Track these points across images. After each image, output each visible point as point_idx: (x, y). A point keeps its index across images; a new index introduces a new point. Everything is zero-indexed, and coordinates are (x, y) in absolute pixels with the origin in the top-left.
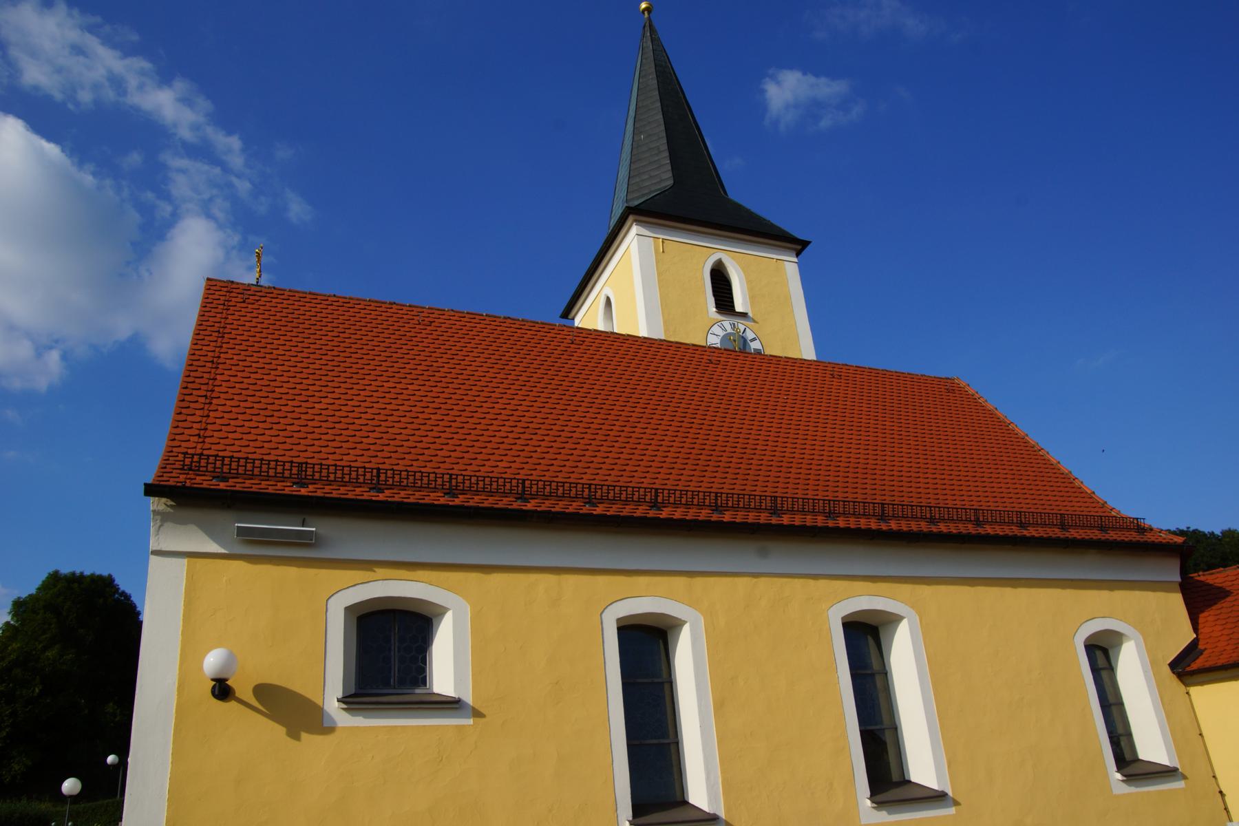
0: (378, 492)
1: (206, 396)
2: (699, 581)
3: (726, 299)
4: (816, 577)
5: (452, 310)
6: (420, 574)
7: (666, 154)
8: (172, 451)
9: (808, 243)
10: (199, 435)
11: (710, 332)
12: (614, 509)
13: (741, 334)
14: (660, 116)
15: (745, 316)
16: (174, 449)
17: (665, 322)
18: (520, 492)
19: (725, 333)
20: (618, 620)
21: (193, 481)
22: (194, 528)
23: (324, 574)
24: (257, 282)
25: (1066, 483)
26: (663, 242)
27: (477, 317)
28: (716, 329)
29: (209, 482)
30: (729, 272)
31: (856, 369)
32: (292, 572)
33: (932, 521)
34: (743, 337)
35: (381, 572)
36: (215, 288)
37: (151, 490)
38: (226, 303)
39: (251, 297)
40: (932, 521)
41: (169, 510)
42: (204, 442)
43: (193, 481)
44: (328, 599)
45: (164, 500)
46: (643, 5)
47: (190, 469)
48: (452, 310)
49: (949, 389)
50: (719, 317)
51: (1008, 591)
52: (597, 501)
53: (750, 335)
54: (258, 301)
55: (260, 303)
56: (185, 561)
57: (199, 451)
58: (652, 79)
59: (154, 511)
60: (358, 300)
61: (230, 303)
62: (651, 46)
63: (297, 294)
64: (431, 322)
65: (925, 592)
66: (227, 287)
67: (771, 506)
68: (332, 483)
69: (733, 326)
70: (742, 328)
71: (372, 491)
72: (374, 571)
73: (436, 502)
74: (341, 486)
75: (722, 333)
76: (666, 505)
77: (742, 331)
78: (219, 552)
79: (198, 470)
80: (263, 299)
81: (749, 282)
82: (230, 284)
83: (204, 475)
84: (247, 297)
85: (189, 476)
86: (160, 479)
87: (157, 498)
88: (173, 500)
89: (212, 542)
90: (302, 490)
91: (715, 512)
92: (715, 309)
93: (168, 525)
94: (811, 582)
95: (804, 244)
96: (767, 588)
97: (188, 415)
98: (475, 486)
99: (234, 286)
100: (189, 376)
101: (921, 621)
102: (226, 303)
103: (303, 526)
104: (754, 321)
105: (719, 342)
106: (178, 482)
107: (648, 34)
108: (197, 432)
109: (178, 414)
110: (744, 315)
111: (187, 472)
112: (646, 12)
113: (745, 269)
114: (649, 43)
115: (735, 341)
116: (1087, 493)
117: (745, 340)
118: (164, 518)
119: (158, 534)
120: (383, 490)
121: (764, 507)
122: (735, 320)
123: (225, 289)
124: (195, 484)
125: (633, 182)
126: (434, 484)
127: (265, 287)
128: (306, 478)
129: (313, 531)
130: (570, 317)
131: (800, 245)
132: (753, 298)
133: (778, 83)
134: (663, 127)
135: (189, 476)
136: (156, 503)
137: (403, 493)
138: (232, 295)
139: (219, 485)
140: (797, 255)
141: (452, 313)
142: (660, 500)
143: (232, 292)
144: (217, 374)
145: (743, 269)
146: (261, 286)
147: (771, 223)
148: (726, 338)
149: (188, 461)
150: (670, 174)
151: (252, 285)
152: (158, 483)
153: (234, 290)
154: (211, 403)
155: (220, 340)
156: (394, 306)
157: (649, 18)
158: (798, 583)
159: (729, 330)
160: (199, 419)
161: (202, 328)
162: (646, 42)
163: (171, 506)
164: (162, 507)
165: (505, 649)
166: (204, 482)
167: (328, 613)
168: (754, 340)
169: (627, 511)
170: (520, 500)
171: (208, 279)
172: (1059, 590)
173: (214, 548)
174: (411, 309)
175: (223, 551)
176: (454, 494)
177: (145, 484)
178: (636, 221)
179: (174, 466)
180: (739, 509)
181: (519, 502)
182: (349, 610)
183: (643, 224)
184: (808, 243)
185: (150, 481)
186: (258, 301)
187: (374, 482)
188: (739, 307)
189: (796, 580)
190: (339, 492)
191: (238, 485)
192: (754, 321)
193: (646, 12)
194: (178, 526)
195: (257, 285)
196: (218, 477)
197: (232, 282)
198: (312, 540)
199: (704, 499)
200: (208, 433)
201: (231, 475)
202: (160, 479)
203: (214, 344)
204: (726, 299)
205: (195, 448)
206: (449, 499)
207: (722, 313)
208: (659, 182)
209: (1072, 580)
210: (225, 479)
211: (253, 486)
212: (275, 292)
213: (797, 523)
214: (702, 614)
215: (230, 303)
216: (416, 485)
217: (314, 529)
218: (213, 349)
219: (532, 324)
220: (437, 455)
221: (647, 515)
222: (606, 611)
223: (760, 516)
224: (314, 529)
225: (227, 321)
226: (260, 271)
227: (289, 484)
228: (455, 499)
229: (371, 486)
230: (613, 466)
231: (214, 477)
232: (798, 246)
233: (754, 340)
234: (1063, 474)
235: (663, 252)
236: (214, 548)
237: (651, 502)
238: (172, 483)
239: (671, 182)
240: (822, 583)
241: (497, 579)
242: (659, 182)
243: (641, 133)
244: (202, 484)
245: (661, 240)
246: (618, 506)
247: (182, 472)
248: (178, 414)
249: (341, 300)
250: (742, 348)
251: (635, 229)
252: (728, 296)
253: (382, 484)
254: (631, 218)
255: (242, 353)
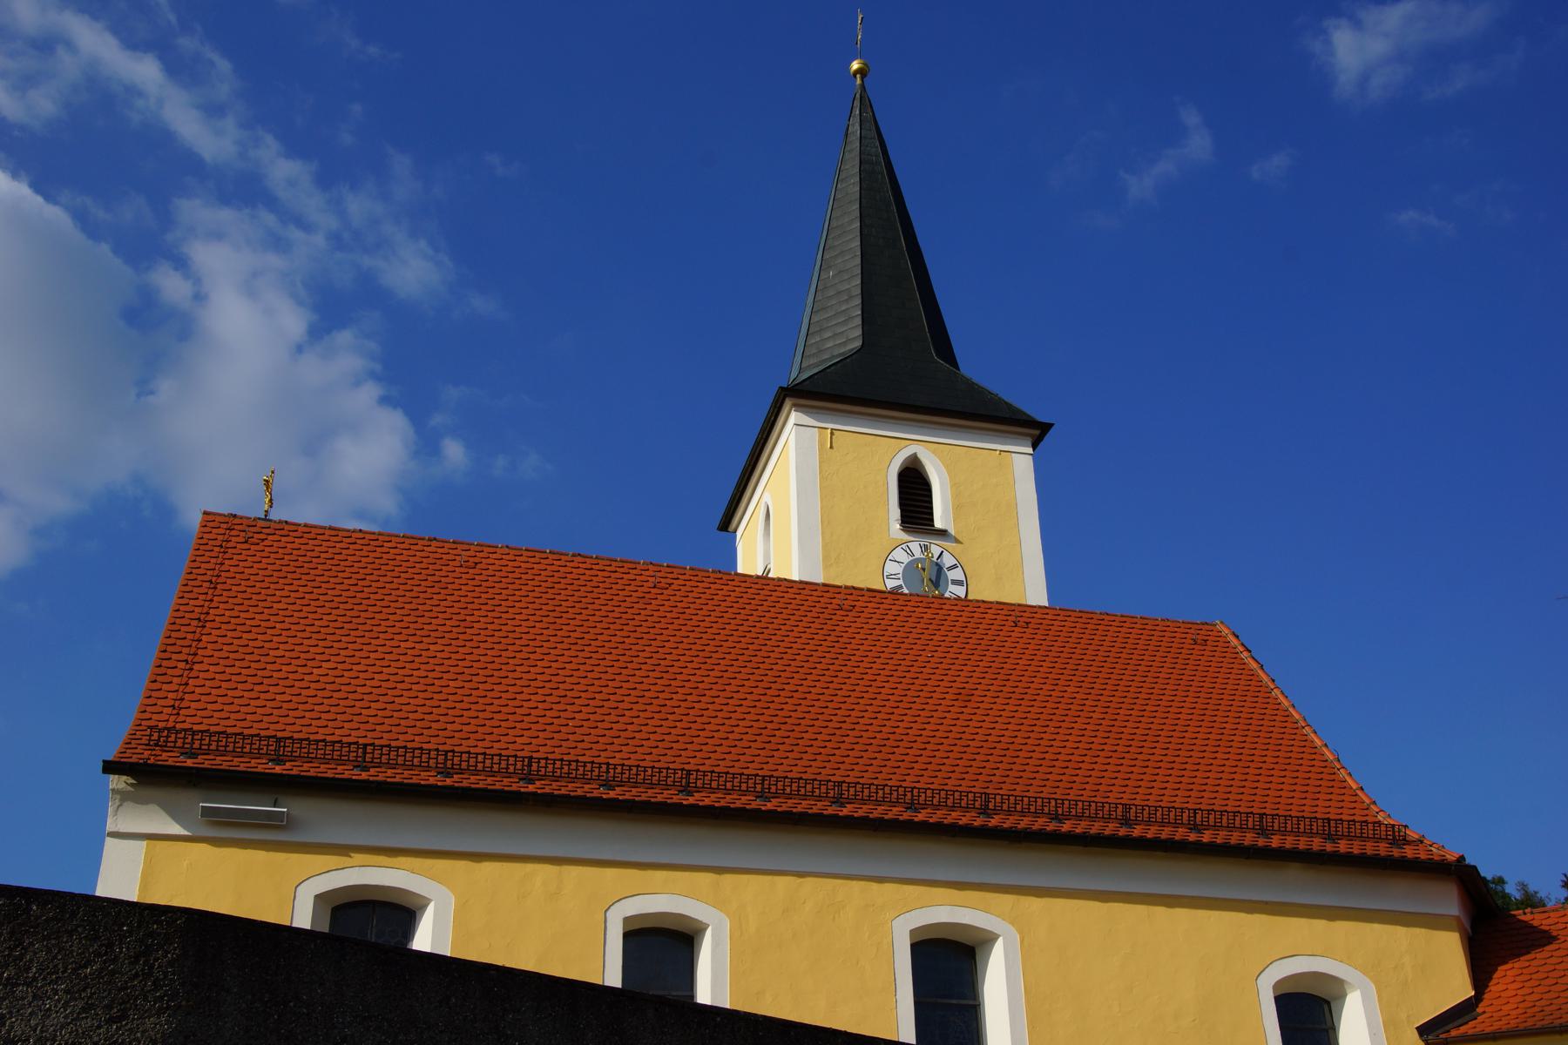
0: (361, 771)
1: (186, 661)
2: (728, 879)
3: (912, 509)
4: (880, 880)
5: (507, 547)
6: (402, 860)
7: (858, 301)
8: (140, 725)
9: (1051, 425)
10: (173, 706)
11: (890, 557)
12: (1025, 822)
13: (935, 559)
14: (856, 243)
15: (944, 535)
16: (143, 723)
17: (825, 546)
18: (683, 784)
19: (911, 558)
20: (627, 920)
21: (159, 758)
22: (156, 808)
23: (295, 858)
24: (266, 516)
25: (1327, 774)
26: (832, 434)
27: (537, 554)
28: (899, 554)
29: (176, 759)
30: (928, 471)
31: (1080, 615)
32: (260, 856)
33: (608, 785)
34: (937, 564)
35: (358, 858)
36: (211, 524)
37: (110, 767)
38: (224, 544)
39: (255, 535)
40: (913, 806)
41: (129, 788)
42: (178, 714)
43: (159, 758)
44: (297, 886)
45: (124, 778)
46: (855, 65)
47: (156, 745)
48: (507, 547)
49: (1202, 636)
50: (905, 537)
51: (1160, 911)
52: (1065, 817)
53: (948, 561)
54: (263, 540)
55: (266, 543)
56: (144, 843)
57: (170, 724)
58: (854, 183)
59: (113, 790)
60: (390, 535)
61: (229, 545)
62: (859, 132)
63: (313, 530)
64: (476, 564)
65: (1034, 905)
66: (227, 523)
67: (1123, 816)
68: (496, 774)
69: (926, 548)
70: (936, 550)
71: (521, 783)
72: (350, 857)
73: (653, 800)
74: (241, 762)
75: (906, 559)
76: (998, 812)
77: (936, 556)
78: (182, 833)
79: (166, 746)
80: (270, 537)
81: (955, 485)
82: (232, 519)
83: (172, 751)
84: (251, 535)
85: (154, 753)
86: (122, 755)
87: (117, 776)
88: (134, 779)
89: (175, 823)
90: (363, 773)
91: (1193, 831)
92: (898, 526)
93: (128, 805)
94: (874, 886)
95: (1045, 428)
96: (813, 890)
97: (163, 683)
98: (589, 773)
99: (236, 521)
100: (170, 637)
101: (1022, 942)
102: (224, 544)
103: (275, 807)
104: (957, 541)
105: (901, 572)
106: (141, 759)
107: (858, 112)
108: (172, 703)
109: (152, 682)
110: (943, 533)
111: (152, 748)
112: (858, 76)
113: (951, 468)
114: (857, 127)
115: (924, 569)
116: (1352, 788)
117: (939, 568)
118: (124, 797)
119: (116, 815)
120: (692, 792)
121: (1315, 831)
122: (925, 541)
123: (225, 526)
124: (159, 760)
125: (813, 341)
126: (628, 774)
127: (275, 522)
128: (283, 755)
129: (284, 812)
130: (732, 528)
131: (1038, 429)
132: (958, 509)
133: (1357, 24)
134: (858, 260)
135: (154, 753)
136: (117, 782)
137: (555, 785)
138: (233, 533)
139: (185, 762)
140: (1034, 446)
141: (507, 551)
142: (991, 806)
143: (233, 529)
144: (202, 634)
145: (947, 466)
146: (270, 520)
147: (1000, 398)
148: (911, 569)
149: (155, 736)
150: (859, 332)
151: (259, 519)
152: (118, 760)
153: (236, 527)
154: (191, 669)
155: (210, 592)
156: (434, 543)
157: (863, 86)
158: (856, 886)
159: (918, 554)
160: (176, 687)
161: (191, 577)
162: (853, 125)
163: (132, 785)
164: (122, 786)
165: (490, 945)
166: (170, 759)
167: (296, 902)
168: (954, 567)
169: (1095, 829)
170: (837, 805)
171: (205, 513)
172: (1243, 915)
173: (177, 829)
174: (455, 546)
175: (186, 833)
176: (611, 786)
177: (104, 761)
178: (794, 405)
179: (139, 742)
180: (1097, 819)
181: (834, 807)
182: (320, 898)
183: (810, 410)
184: (1051, 425)
185: (110, 758)
186: (263, 540)
187: (525, 772)
188: (938, 524)
189: (854, 882)
190: (502, 783)
191: (206, 762)
192: (957, 541)
193: (858, 76)
194: (139, 806)
195: (265, 519)
196: (186, 753)
197: (235, 516)
198: (282, 822)
199: (947, 798)
200: (184, 704)
201: (202, 752)
202: (122, 755)
203: (203, 597)
204: (912, 509)
205: (168, 720)
206: (683, 797)
207: (908, 531)
208: (844, 344)
209: (1267, 903)
210: (193, 755)
211: (222, 762)
212: (287, 527)
213: (1302, 846)
214: (728, 916)
215: (229, 545)
216: (571, 776)
217: (285, 810)
218: (202, 603)
219: (608, 563)
220: (647, 724)
221: (945, 820)
222: (612, 907)
223: (1285, 839)
224: (285, 810)
225: (223, 568)
226: (271, 500)
227: (264, 761)
228: (610, 792)
229: (182, 750)
230: (979, 750)
231: (182, 754)
232: (1035, 431)
233: (954, 567)
234: (1327, 761)
235: (831, 447)
236: (177, 829)
237: (834, 797)
238: (134, 760)
239: (858, 344)
240: (889, 887)
241: (488, 868)
242: (844, 344)
243: (830, 267)
244: (239, 766)
245: (829, 431)
246: (1030, 819)
247: (148, 747)
248: (152, 682)
249: (367, 536)
250: (934, 579)
251: (795, 417)
252: (907, 514)
253: (534, 775)
254: (788, 403)
255: (356, 564)
